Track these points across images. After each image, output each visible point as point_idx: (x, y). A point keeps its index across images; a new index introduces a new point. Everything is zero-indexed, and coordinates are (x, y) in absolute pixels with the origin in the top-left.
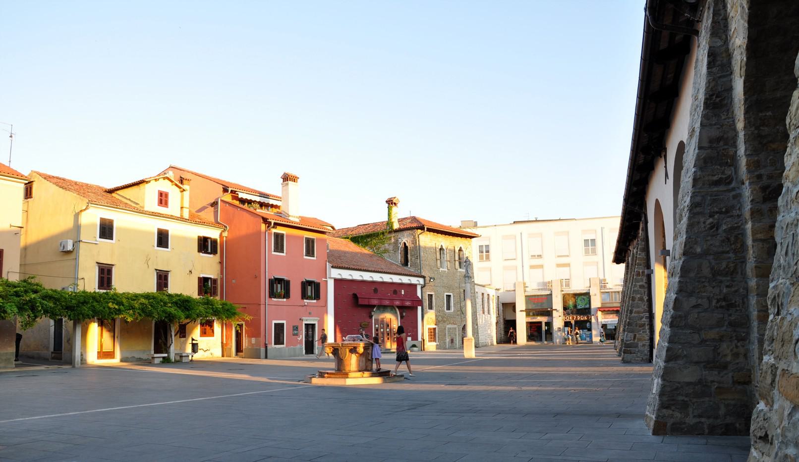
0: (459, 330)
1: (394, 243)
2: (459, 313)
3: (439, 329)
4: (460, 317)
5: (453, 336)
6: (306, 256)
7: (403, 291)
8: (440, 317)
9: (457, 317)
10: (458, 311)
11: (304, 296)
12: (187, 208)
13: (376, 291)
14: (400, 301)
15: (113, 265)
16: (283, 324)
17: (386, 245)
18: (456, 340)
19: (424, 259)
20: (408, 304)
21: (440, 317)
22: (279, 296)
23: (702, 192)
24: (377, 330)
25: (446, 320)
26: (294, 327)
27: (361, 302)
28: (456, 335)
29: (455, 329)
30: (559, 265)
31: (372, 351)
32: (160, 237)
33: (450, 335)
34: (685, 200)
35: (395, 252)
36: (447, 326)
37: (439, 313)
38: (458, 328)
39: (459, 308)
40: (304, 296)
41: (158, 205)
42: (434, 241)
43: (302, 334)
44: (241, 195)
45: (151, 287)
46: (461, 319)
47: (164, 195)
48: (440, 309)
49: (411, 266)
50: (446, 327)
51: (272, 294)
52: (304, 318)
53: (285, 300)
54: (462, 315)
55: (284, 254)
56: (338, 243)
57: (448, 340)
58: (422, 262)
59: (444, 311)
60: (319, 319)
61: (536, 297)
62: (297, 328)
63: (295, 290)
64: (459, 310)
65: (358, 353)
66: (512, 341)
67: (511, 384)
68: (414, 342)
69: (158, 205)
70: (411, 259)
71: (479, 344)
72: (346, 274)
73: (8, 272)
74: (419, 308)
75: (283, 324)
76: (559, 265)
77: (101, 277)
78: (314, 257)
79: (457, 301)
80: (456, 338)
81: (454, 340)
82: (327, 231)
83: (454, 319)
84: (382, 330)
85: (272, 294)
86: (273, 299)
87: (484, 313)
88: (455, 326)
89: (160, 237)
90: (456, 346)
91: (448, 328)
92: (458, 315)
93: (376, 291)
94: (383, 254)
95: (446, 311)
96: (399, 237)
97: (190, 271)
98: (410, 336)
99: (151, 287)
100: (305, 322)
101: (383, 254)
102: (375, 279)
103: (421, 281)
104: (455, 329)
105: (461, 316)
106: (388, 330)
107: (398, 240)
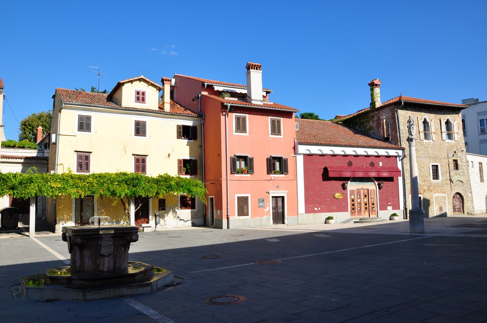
0: (449, 199)
1: (377, 120)
5: (441, 204)
6: (271, 134)
9: (446, 186)
11: (269, 171)
12: (168, 103)
13: (350, 164)
14: (363, 172)
15: (91, 152)
16: (248, 197)
17: (371, 123)
20: (385, 175)
21: (425, 187)
22: (242, 172)
24: (353, 201)
25: (432, 189)
26: (259, 200)
27: (331, 175)
28: (445, 203)
32: (81, 123)
33: (438, 204)
35: (378, 128)
37: (423, 183)
40: (269, 171)
41: (136, 102)
43: (269, 206)
44: (216, 88)
45: (129, 168)
47: (141, 93)
49: (392, 139)
50: (433, 196)
51: (234, 170)
52: (270, 192)
53: (249, 175)
55: (247, 134)
56: (304, 121)
58: (401, 135)
60: (287, 191)
62: (263, 200)
63: (260, 166)
65: (115, 263)
68: (395, 211)
69: (136, 102)
70: (392, 133)
71: (474, 211)
72: (315, 150)
74: (400, 179)
75: (248, 197)
77: (88, 160)
78: (281, 135)
82: (294, 111)
83: (442, 188)
84: (359, 200)
85: (234, 170)
86: (235, 175)
88: (444, 195)
89: (81, 123)
91: (436, 197)
92: (446, 184)
93: (350, 164)
94: (368, 132)
95: (249, 195)
96: (380, 114)
97: (169, 155)
98: (390, 205)
99: (129, 168)
100: (272, 195)
101: (368, 132)
103: (400, 152)
104: (444, 197)
106: (365, 200)
107: (380, 118)
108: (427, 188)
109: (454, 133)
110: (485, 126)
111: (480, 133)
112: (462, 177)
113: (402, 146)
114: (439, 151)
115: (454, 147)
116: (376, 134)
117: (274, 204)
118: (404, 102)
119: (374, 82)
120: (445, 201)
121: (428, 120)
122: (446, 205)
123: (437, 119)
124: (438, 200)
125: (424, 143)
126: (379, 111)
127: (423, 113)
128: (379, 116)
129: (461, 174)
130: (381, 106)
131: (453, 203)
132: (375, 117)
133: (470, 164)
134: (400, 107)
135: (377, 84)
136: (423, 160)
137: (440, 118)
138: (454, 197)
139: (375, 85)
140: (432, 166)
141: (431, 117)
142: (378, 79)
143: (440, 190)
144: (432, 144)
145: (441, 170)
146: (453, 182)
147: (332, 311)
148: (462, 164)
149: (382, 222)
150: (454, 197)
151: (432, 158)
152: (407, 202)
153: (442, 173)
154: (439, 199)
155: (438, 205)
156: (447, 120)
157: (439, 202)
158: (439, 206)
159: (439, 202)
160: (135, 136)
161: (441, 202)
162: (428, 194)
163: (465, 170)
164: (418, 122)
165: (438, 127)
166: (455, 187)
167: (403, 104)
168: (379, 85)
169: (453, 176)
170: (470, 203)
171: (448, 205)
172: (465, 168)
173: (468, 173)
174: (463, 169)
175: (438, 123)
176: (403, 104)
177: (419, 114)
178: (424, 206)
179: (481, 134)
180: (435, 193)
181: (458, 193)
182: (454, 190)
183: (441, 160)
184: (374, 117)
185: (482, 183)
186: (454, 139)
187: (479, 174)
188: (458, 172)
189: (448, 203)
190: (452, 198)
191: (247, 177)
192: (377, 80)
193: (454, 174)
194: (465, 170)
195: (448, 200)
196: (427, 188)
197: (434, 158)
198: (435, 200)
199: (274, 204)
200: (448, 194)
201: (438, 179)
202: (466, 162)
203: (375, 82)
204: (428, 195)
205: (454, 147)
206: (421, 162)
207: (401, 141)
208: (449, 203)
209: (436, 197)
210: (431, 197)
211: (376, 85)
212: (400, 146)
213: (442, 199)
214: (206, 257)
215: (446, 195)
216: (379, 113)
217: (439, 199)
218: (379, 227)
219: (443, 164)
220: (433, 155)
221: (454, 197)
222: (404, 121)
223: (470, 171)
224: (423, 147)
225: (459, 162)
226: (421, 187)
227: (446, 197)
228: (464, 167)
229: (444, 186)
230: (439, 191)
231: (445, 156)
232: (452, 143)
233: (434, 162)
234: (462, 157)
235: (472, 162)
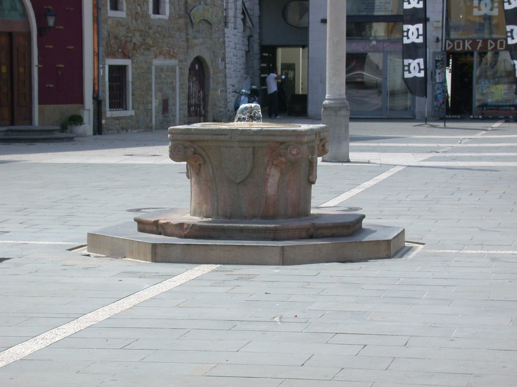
2: (182, 21)
3: (135, 68)
4: (183, 35)
7: (73, 47)
9: (178, 34)
10: (180, 17)
18: (174, 105)
21: (137, 34)
28: (174, 89)
29: (173, 70)
38: (181, 68)
39: (183, 9)
46: (187, 40)
50: (151, 64)
54: (190, 31)
57: (155, 103)
61: (113, 257)
64: (182, 13)
66: (264, 65)
67: (412, 147)
80: (174, 98)
81: (170, 102)
88: (173, 62)
91: (157, 67)
104: (173, 70)
105: (187, 34)
112: (211, 10)
117: (275, 125)
147: (3, 220)
152: (309, 73)
166: (195, 41)
170: (221, 91)
178: (133, 95)
185: (320, 20)
191: (217, 243)
195: (180, 80)
198: (156, 78)
199: (275, 125)
201: (161, 11)
208: (181, 88)
218: (210, 224)
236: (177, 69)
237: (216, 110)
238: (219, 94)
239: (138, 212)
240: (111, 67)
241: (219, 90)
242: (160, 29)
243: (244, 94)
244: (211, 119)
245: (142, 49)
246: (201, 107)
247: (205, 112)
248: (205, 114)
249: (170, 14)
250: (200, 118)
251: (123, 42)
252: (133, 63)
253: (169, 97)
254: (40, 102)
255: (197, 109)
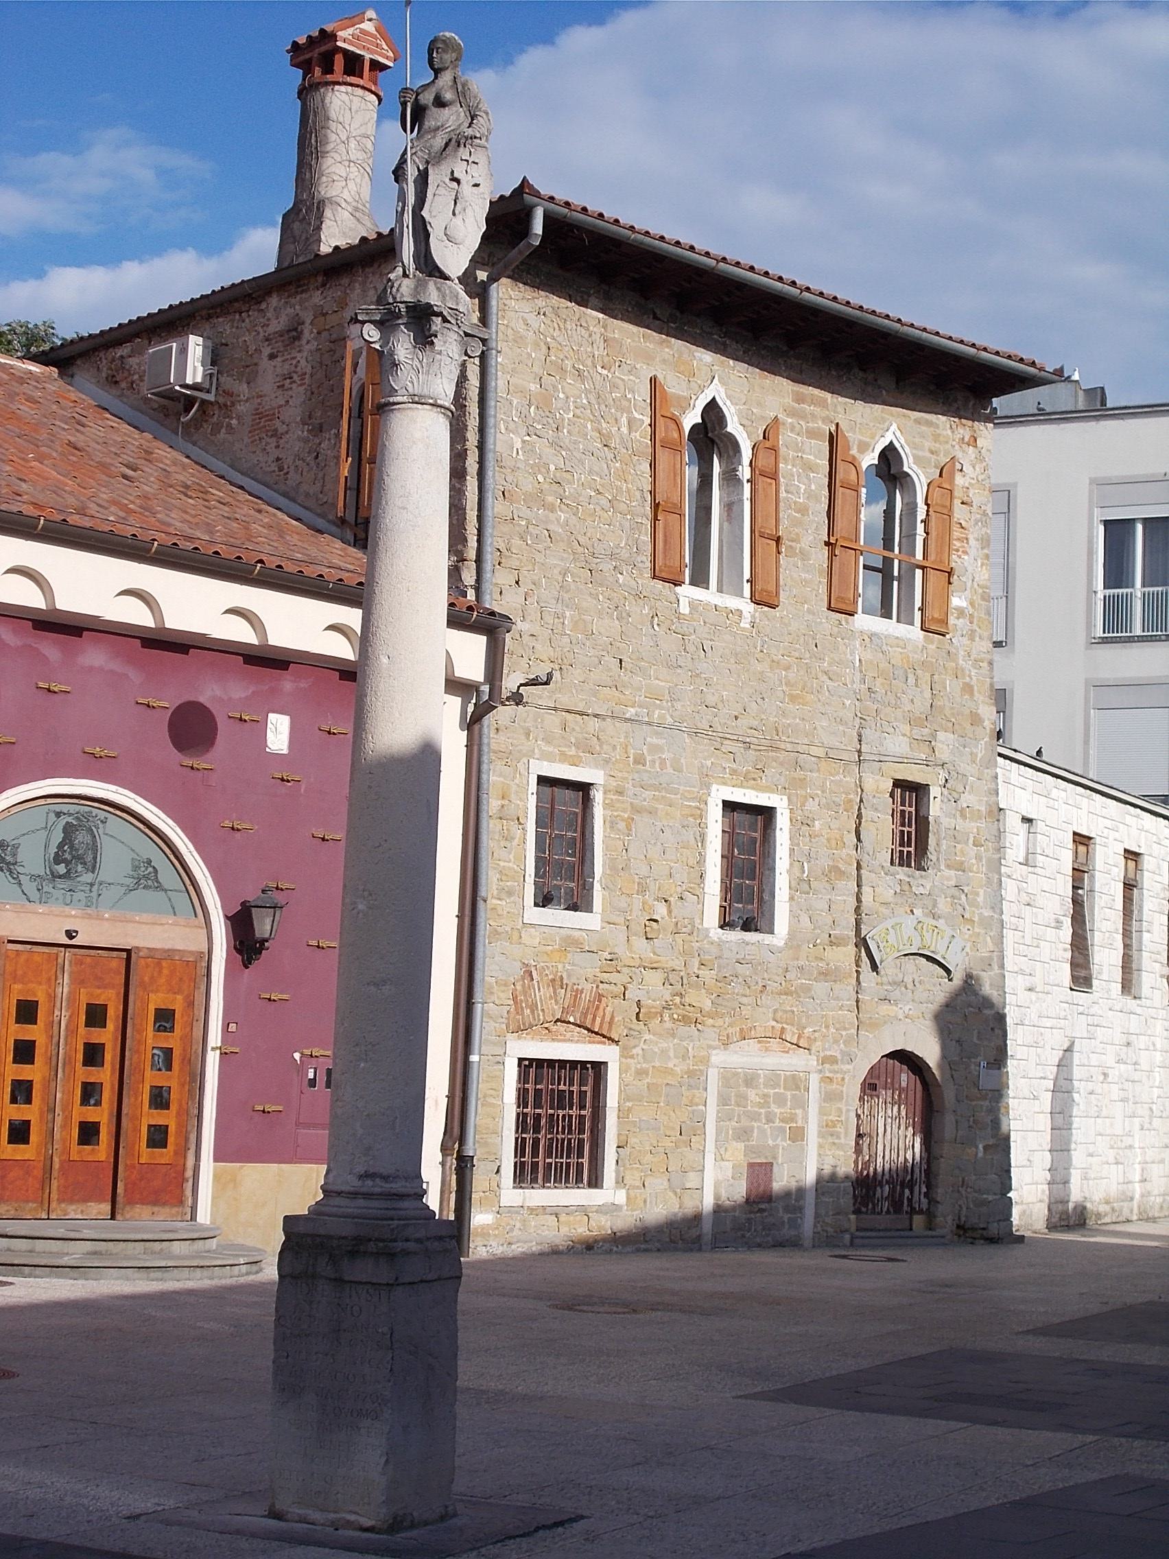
0: (829, 1097)
8: (654, 978)
9: (820, 988)
10: (833, 942)
19: (527, 484)
23: (334, 1206)
25: (707, 1005)
28: (798, 1135)
30: (1128, 985)
31: (1126, 869)
33: (743, 1134)
34: (896, 994)
36: (719, 1058)
37: (640, 943)
42: (649, 358)
48: (661, 911)
50: (706, 1061)
58: (496, 507)
59: (688, 929)
73: (829, 608)
76: (1128, 985)
79: (825, 862)
83: (789, 1002)
87: (1082, 977)
88: (797, 1061)
90: (794, 1224)
91: (728, 1077)
92: (825, 975)
102: (70, 601)
104: (796, 1083)
108: (666, 993)
109: (923, 568)
110: (1133, 586)
111: (1099, 633)
112: (949, 932)
113: (492, 602)
114: (793, 698)
115: (911, 680)
116: (293, 478)
118: (547, 217)
119: (333, 37)
120: (799, 1112)
121: (733, 426)
122: (802, 1150)
123: (812, 434)
124: (742, 1099)
125: (684, 609)
126: (345, 281)
127: (705, 357)
128: (341, 325)
129: (943, 906)
130: (364, 239)
131: (859, 1136)
132: (307, 335)
133: (1016, 838)
134: (517, 254)
135: (360, 58)
136: (655, 749)
137: (833, 429)
138: (873, 1087)
139: (339, 61)
140: (730, 807)
141: (759, 404)
142: (371, 14)
143: (765, 1022)
144: (745, 624)
145: (792, 850)
146: (874, 967)
148: (961, 824)
149: (158, 1274)
150: (870, 1087)
151: (729, 746)
153: (800, 885)
154: (752, 1095)
155: (741, 1146)
156: (883, 455)
157: (755, 1117)
158: (748, 1150)
159: (755, 1117)
160: (516, 1061)
161: (769, 1120)
162: (668, 1044)
163: (978, 875)
164: (653, 425)
165: (810, 495)
166: (885, 1009)
167: (538, 227)
168: (376, 66)
169: (883, 909)
170: (985, 1148)
171: (820, 1146)
172: (979, 858)
173: (997, 903)
174: (961, 867)
175: (809, 467)
176: (538, 227)
177: (664, 361)
179: (1104, 641)
180: (726, 1045)
181: (903, 1057)
182: (875, 1025)
183: (799, 774)
184: (298, 338)
186: (918, 615)
187: (1068, 922)
188: (923, 883)
189: (821, 1135)
190: (854, 1089)
192: (368, 26)
193: (888, 895)
194: (978, 875)
195: (822, 1112)
196: (666, 993)
197: (748, 745)
198: (723, 1100)
200: (832, 1060)
202: (990, 813)
203: (346, 39)
204: (664, 1052)
205: (911, 680)
206: (639, 760)
207: (489, 558)
208: (828, 1130)
209: (728, 1077)
210: (691, 1074)
211: (353, 64)
212: (471, 595)
213: (780, 1100)
214: (578, 1307)
215: (813, 1062)
216: (343, 304)
217: (752, 1095)
219: (811, 805)
220: (744, 722)
221: (873, 1087)
222: (534, 387)
223: (1010, 890)
224: (669, 644)
225: (936, 808)
226: (614, 977)
227: (814, 1080)
228: (972, 851)
229: (808, 989)
230: (760, 1032)
231: (833, 741)
232: (901, 643)
233: (747, 780)
234: (965, 767)
235: (1028, 820)
236: (814, 1080)
237: (967, 1198)
238: (980, 1154)
239: (372, 521)
240: (528, 1066)
241: (981, 1147)
242: (744, 970)
243: (463, 1165)
244: (950, 1222)
245: (666, 1018)
246: (916, 1189)
247: (929, 1203)
248: (928, 1209)
249: (792, 935)
250: (323, 1126)
251: (586, 997)
252: (624, 1053)
253: (775, 1158)
254: (220, 1155)
255: (902, 1193)
